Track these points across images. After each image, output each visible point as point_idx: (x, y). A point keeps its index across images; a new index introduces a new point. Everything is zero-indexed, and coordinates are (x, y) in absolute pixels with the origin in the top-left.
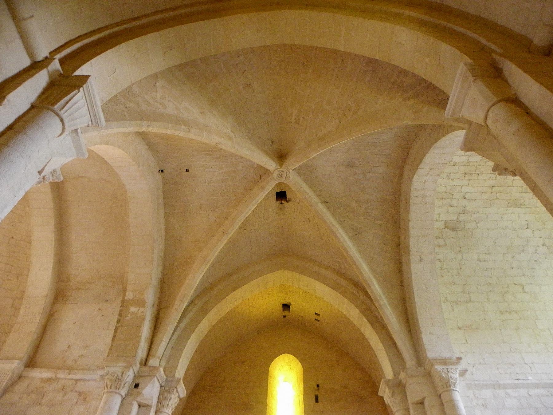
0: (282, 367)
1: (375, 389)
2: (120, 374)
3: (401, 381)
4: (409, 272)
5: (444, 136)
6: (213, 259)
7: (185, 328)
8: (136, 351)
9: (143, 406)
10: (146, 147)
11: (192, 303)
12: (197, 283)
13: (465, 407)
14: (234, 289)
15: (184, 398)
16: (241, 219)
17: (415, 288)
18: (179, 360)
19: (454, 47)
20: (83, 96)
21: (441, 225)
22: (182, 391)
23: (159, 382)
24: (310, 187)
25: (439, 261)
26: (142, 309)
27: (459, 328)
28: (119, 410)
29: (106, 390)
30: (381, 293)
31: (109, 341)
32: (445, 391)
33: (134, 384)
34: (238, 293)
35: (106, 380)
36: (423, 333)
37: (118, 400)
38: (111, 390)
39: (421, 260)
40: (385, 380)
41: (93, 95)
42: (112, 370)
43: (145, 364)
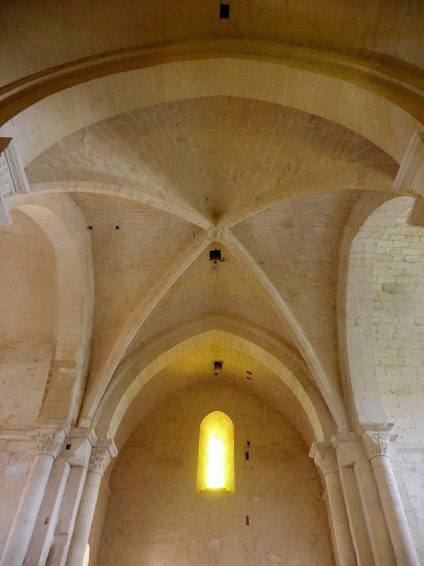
0: (213, 424)
1: (306, 449)
2: (51, 436)
3: (332, 444)
4: (344, 336)
5: (388, 200)
6: (144, 320)
7: (117, 388)
8: (67, 413)
9: (76, 467)
10: (74, 203)
11: (123, 363)
12: (128, 344)
13: (394, 472)
14: (166, 349)
15: (115, 457)
16: (173, 279)
17: (350, 353)
18: (110, 420)
19: (407, 111)
20: (4, 161)
21: (379, 287)
22: (114, 450)
23: (91, 443)
24: (245, 247)
25: (375, 324)
26: (72, 370)
27: (392, 392)
28: (51, 471)
29: (38, 452)
30: (315, 357)
31: (39, 401)
32: (375, 456)
33: (66, 446)
34: (170, 352)
35: (37, 442)
36: (356, 398)
37: (50, 461)
38: (43, 452)
39: (356, 324)
40: (316, 443)
41: (16, 159)
42: (43, 432)
43: (76, 426)
